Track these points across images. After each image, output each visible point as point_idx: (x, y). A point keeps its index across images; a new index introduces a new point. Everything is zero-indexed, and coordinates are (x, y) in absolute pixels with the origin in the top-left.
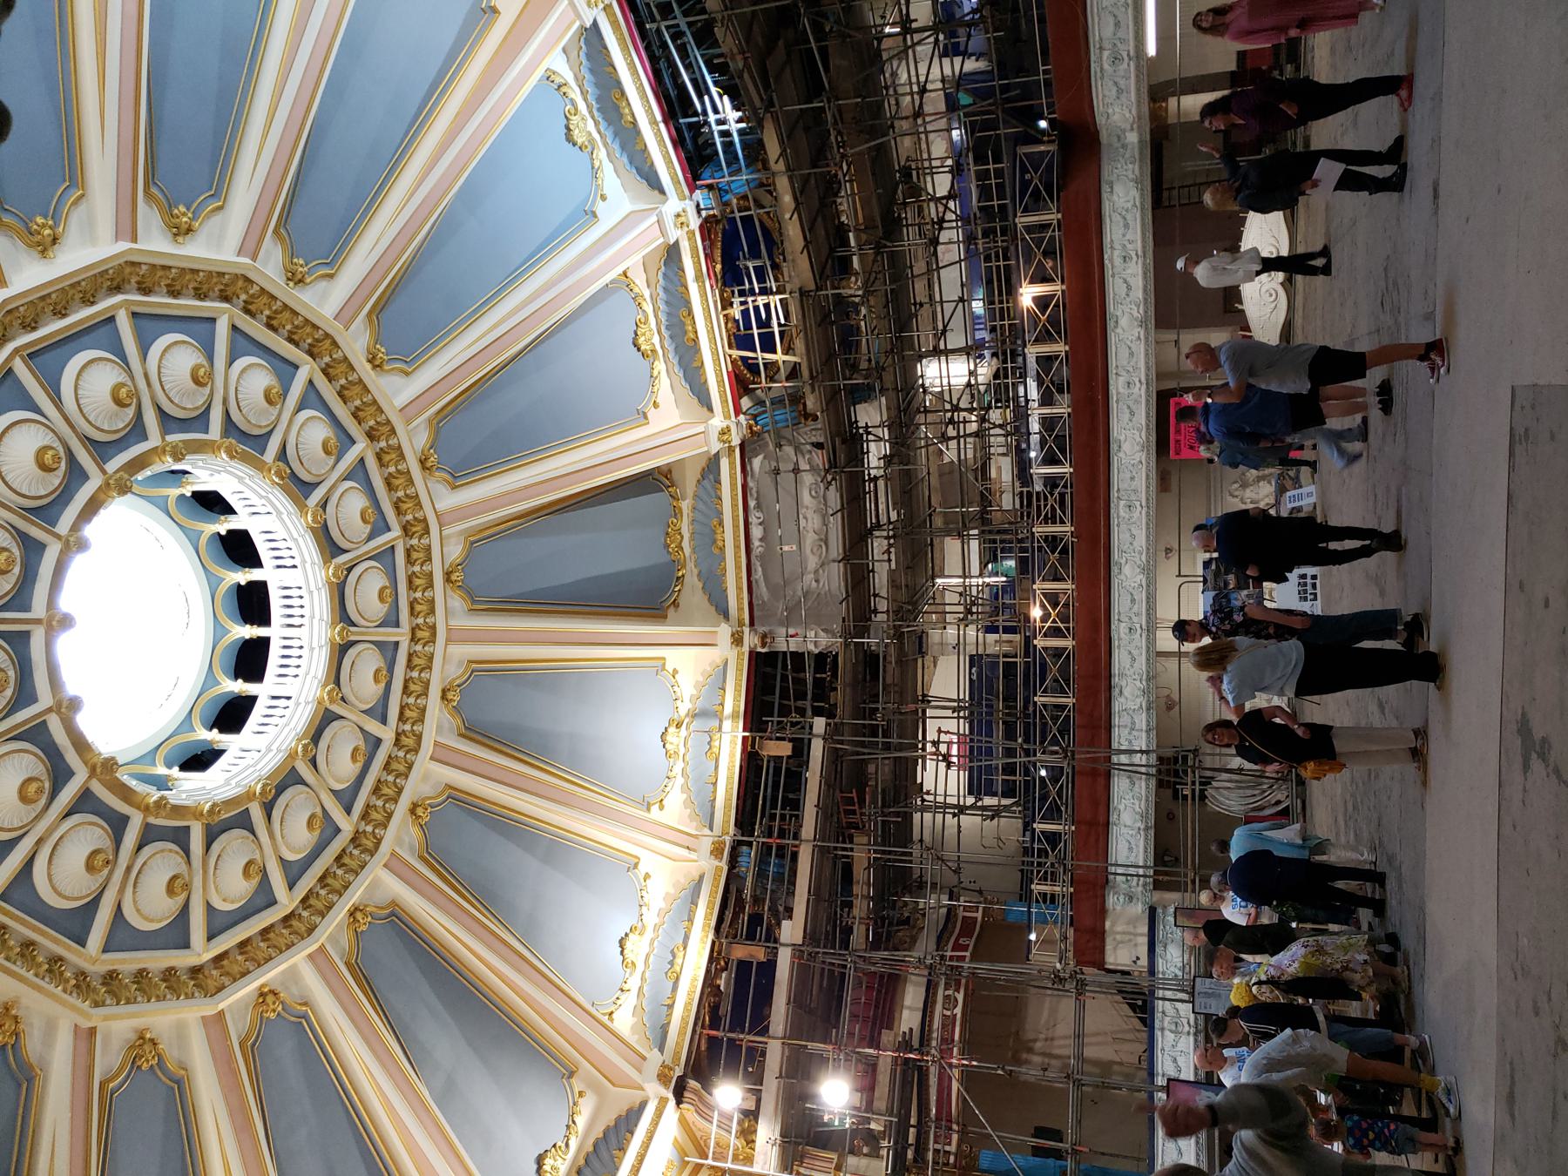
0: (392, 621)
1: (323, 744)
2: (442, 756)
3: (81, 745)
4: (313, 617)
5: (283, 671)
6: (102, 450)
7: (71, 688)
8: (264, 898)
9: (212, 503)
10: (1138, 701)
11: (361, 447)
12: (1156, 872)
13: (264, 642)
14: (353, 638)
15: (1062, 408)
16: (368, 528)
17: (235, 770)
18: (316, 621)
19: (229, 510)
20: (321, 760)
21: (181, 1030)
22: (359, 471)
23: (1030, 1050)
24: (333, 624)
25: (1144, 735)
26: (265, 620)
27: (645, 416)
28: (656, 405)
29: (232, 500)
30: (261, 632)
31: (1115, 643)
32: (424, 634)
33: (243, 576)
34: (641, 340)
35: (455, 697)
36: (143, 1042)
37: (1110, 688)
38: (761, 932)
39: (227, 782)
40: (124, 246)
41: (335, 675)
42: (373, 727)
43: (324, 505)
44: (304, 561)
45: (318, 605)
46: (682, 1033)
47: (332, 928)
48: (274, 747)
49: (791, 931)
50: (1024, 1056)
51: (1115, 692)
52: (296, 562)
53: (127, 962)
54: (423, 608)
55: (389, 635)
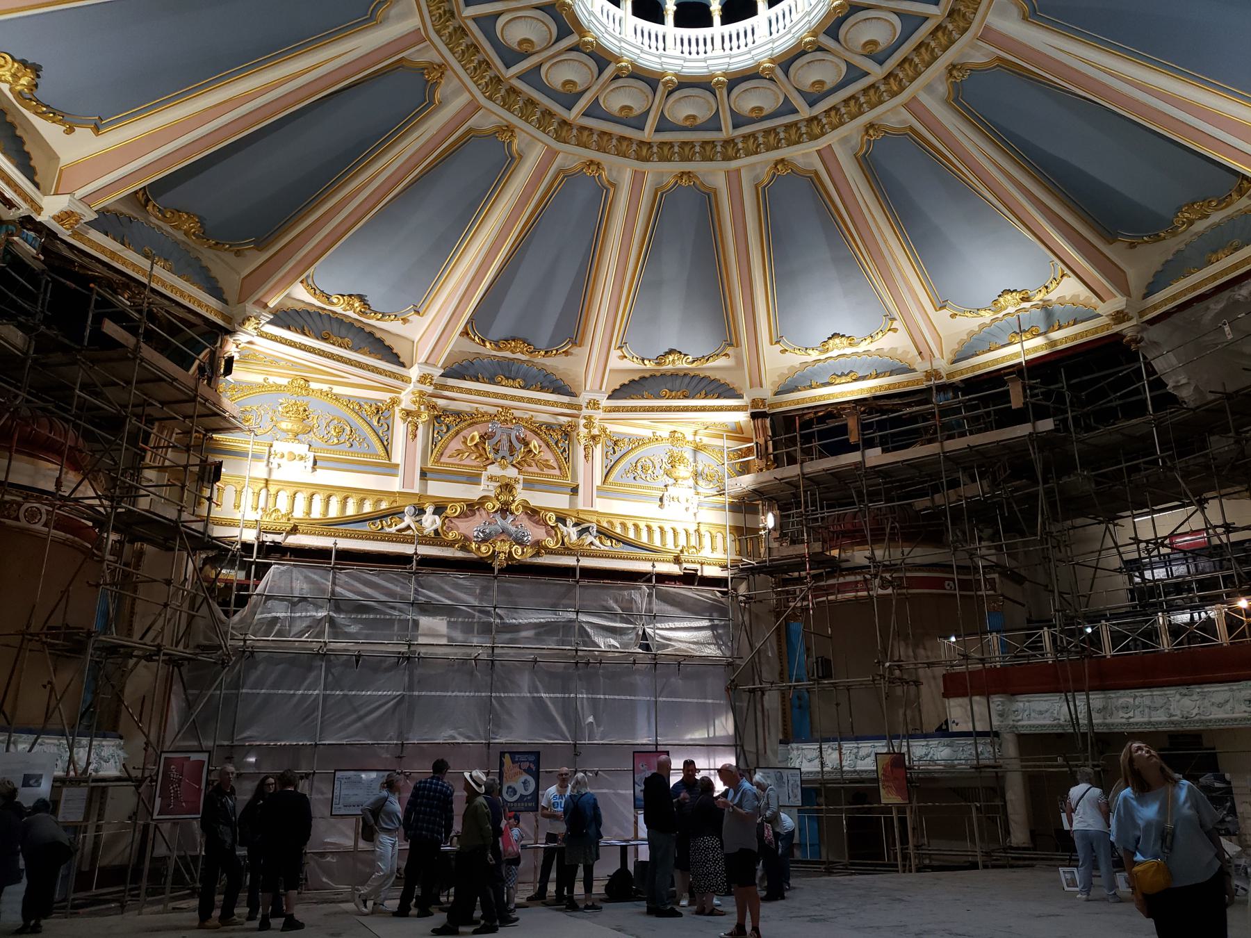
0: (664, 125)
1: (631, 81)
2: (734, 178)
4: (730, 57)
10: (1178, 713)
11: (877, 72)
12: (1084, 735)
13: (709, 23)
14: (661, 87)
15: (1165, 644)
16: (807, 89)
18: (727, 60)
20: (620, 82)
22: (855, 74)
24: (725, 74)
25: (1146, 719)
26: (679, 22)
27: (942, 308)
30: (717, 19)
31: (1235, 686)
32: (644, 152)
34: (837, 341)
35: (684, 182)
37: (1187, 684)
38: (870, 434)
39: (591, 13)
42: (651, 122)
43: (820, 49)
44: (730, 57)
45: (740, 60)
46: (973, 368)
47: (436, 51)
48: (623, 44)
49: (875, 456)
51: (1183, 690)
52: (775, 35)
54: (665, 152)
55: (726, 120)
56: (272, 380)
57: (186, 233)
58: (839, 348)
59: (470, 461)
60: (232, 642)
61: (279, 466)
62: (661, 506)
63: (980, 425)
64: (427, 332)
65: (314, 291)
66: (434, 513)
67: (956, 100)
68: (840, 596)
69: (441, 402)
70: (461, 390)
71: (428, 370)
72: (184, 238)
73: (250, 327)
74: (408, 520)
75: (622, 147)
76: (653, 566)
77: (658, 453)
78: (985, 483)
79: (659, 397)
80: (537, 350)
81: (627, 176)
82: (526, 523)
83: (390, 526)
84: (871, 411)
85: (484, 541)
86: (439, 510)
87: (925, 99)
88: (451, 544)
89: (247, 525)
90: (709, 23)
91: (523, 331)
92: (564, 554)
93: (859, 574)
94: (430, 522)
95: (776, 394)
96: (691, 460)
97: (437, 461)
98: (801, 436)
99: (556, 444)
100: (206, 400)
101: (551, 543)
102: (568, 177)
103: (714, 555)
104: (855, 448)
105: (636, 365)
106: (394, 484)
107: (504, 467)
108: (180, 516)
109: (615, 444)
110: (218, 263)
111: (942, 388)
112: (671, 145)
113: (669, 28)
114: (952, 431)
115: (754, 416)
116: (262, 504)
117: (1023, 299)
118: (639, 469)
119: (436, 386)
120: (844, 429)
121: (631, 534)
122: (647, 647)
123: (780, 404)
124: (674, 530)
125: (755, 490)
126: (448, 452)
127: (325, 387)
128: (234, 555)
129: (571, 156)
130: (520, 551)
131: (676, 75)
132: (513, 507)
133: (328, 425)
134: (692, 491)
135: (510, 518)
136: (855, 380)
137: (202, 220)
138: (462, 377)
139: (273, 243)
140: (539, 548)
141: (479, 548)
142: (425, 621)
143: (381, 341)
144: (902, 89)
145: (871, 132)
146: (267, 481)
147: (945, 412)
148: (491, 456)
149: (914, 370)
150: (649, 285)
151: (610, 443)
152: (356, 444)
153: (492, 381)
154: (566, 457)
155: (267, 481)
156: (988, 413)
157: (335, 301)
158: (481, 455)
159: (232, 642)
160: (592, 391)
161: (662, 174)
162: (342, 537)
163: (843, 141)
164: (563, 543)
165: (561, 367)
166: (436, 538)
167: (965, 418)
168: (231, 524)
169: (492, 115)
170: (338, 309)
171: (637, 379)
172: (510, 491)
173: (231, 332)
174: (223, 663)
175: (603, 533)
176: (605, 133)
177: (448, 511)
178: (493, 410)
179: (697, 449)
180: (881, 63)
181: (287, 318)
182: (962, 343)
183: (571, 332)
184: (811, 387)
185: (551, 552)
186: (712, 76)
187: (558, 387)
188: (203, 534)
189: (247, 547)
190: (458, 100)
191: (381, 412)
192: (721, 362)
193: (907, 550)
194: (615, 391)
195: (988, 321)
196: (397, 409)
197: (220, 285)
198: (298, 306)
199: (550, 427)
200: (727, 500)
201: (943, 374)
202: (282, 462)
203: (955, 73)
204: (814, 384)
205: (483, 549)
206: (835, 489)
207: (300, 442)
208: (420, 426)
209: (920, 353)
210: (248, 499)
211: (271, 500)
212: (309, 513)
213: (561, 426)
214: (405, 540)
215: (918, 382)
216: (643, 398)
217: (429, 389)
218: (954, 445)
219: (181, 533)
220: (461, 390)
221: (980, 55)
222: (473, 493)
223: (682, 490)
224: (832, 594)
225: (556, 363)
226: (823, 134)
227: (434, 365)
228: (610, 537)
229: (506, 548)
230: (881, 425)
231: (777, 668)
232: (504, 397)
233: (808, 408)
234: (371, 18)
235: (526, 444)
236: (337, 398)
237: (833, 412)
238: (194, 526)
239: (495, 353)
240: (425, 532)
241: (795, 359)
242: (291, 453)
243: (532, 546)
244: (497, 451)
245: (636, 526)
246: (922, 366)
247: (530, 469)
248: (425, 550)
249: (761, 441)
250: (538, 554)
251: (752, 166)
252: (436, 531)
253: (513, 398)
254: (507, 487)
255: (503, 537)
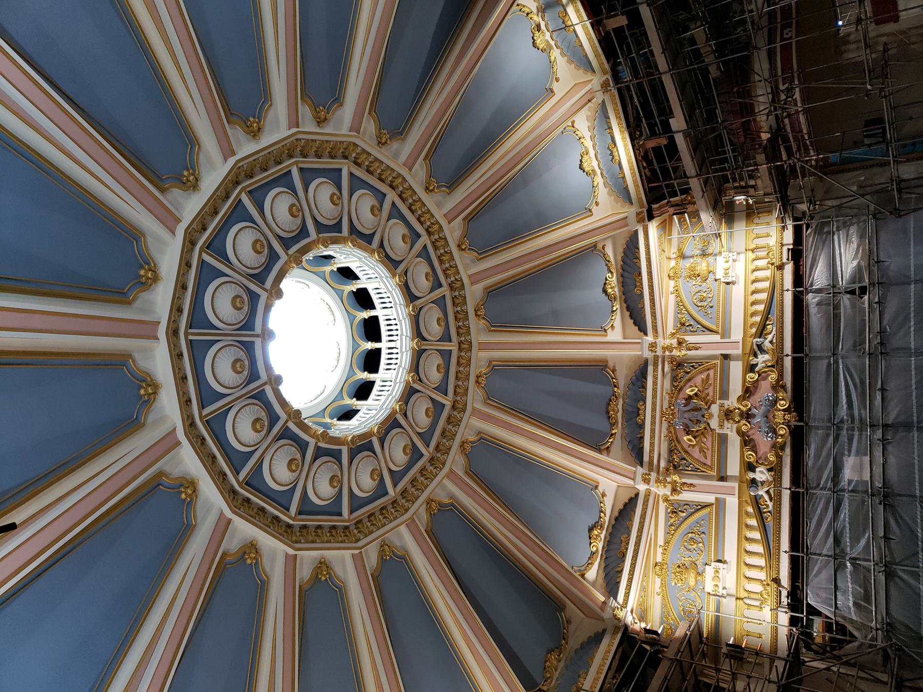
0: (446, 337)
3: (283, 403)
5: (389, 367)
6: (287, 243)
7: (277, 371)
8: (381, 491)
9: (347, 274)
13: (378, 351)
14: (423, 347)
17: (363, 420)
19: (357, 278)
20: (409, 413)
21: (343, 560)
22: (394, 212)
23: (848, 42)
26: (378, 339)
28: (597, 204)
29: (357, 271)
32: (465, 346)
33: (366, 314)
34: (585, 165)
36: (322, 566)
38: (659, 128)
40: (294, 130)
41: (415, 367)
43: (381, 245)
44: (402, 335)
45: (404, 328)
47: (419, 510)
49: (678, 123)
50: (843, 48)
53: (312, 521)
54: (464, 331)
55: (446, 346)
56: (658, 590)
57: (559, 661)
58: (592, 163)
59: (708, 441)
60: (879, 639)
61: (724, 588)
62: (733, 283)
63: (642, 39)
64: (608, 479)
65: (589, 564)
66: (754, 471)
67: (401, 133)
68: (805, 131)
69: (663, 464)
70: (652, 451)
71: (639, 478)
72: (563, 662)
73: (620, 614)
74: (762, 492)
75: (464, 362)
76: (788, 290)
77: (689, 288)
78: (692, 27)
79: (641, 295)
80: (614, 394)
81: (483, 354)
82: (757, 398)
83: (767, 506)
84: (639, 126)
85: (774, 431)
86: (751, 468)
87: (403, 157)
88: (780, 458)
89: (776, 619)
90: (375, 319)
91: (602, 407)
92: (782, 367)
93: (783, 121)
94: (761, 474)
95: (631, 203)
96: (692, 260)
97: (711, 468)
98: (664, 180)
99: (688, 373)
100: (679, 651)
101: (773, 376)
102: (489, 398)
103: (773, 235)
104: (672, 140)
105: (618, 318)
106: (732, 502)
107: (711, 416)
108: (775, 683)
109: (683, 324)
110: (576, 638)
111: (616, 77)
112: (458, 328)
113: (383, 345)
114: (650, 64)
115: (651, 217)
116: (757, 603)
117: (539, 30)
118: (703, 303)
119: (651, 470)
120: (657, 150)
121: (761, 307)
122: (863, 290)
123: (640, 199)
124: (754, 271)
125: (714, 209)
126: (703, 459)
127: (660, 551)
128: (802, 633)
129: (475, 398)
130: (782, 402)
131: (413, 340)
132: (744, 409)
133: (689, 550)
134: (718, 258)
135: (754, 411)
136: (615, 145)
137: (550, 651)
138: (641, 450)
139: (557, 598)
140: (778, 386)
141: (782, 436)
142: (848, 474)
143: (621, 512)
144: (399, 175)
145: (431, 188)
146: (737, 598)
147: (635, 73)
148: (703, 426)
149: (603, 101)
150: (557, 320)
151: (683, 330)
152: (701, 529)
153: (642, 426)
154: (698, 364)
155: (737, 598)
156: (631, 35)
157: (595, 549)
158: (703, 434)
159: (879, 639)
160: (642, 350)
161: (479, 330)
162: (779, 546)
163: (440, 206)
164: (772, 366)
165: (625, 372)
166: (775, 470)
167: (638, 54)
168: (775, 631)
169: (455, 461)
170: (600, 545)
171: (628, 314)
172: (731, 411)
173: (626, 627)
174: (898, 650)
175: (761, 332)
176: (457, 377)
177: (752, 460)
178: (665, 425)
179: (683, 256)
180: (385, 195)
181: (611, 587)
182: (578, 67)
183: (598, 370)
184: (624, 177)
185: (781, 376)
186: (410, 315)
187: (641, 374)
188: (787, 661)
189: (793, 622)
190: (450, 485)
191: (675, 510)
192: (609, 251)
193: (757, 78)
194: (640, 330)
195: (559, 51)
196: (671, 498)
197: (593, 635)
198: (602, 575)
199: (674, 379)
200: (724, 230)
201: (604, 78)
202: (720, 585)
203: (383, 140)
204: (621, 176)
205: (781, 432)
206: (707, 149)
207: (704, 571)
208: (684, 480)
209: (589, 101)
210: (753, 613)
211: (752, 596)
212: (761, 568)
213: (673, 370)
214: (779, 495)
215: (612, 96)
216: (643, 307)
217: (653, 475)
218: (662, 63)
219: (788, 684)
220: (652, 451)
221: (370, 126)
222: (734, 442)
223: (720, 265)
224: (803, 136)
225: (622, 378)
226: (437, 222)
227: (635, 473)
228: (765, 326)
229: (780, 414)
230: (649, 115)
231: (876, 170)
232: (653, 417)
233: (641, 176)
234: (404, 558)
235: (690, 398)
236: (667, 542)
237: (643, 158)
238: (781, 670)
239: (620, 425)
240: (771, 479)
241: (603, 193)
242: (713, 579)
243: (777, 392)
244: (698, 421)
245: (753, 304)
246: (599, 97)
247: (711, 394)
248: (786, 481)
249: (672, 210)
250: (784, 387)
251: (466, 267)
252: (769, 470)
253: (654, 410)
254: (728, 414)
255: (771, 417)
